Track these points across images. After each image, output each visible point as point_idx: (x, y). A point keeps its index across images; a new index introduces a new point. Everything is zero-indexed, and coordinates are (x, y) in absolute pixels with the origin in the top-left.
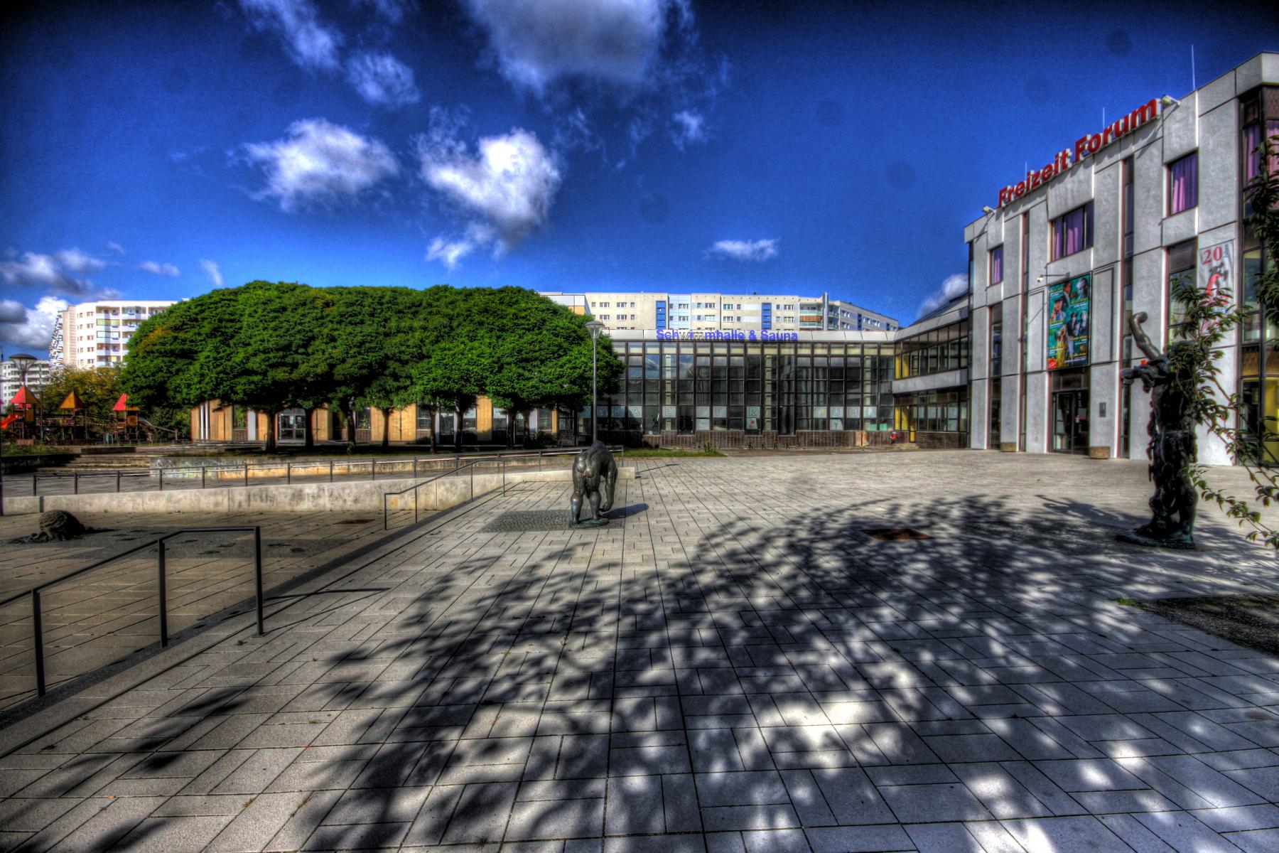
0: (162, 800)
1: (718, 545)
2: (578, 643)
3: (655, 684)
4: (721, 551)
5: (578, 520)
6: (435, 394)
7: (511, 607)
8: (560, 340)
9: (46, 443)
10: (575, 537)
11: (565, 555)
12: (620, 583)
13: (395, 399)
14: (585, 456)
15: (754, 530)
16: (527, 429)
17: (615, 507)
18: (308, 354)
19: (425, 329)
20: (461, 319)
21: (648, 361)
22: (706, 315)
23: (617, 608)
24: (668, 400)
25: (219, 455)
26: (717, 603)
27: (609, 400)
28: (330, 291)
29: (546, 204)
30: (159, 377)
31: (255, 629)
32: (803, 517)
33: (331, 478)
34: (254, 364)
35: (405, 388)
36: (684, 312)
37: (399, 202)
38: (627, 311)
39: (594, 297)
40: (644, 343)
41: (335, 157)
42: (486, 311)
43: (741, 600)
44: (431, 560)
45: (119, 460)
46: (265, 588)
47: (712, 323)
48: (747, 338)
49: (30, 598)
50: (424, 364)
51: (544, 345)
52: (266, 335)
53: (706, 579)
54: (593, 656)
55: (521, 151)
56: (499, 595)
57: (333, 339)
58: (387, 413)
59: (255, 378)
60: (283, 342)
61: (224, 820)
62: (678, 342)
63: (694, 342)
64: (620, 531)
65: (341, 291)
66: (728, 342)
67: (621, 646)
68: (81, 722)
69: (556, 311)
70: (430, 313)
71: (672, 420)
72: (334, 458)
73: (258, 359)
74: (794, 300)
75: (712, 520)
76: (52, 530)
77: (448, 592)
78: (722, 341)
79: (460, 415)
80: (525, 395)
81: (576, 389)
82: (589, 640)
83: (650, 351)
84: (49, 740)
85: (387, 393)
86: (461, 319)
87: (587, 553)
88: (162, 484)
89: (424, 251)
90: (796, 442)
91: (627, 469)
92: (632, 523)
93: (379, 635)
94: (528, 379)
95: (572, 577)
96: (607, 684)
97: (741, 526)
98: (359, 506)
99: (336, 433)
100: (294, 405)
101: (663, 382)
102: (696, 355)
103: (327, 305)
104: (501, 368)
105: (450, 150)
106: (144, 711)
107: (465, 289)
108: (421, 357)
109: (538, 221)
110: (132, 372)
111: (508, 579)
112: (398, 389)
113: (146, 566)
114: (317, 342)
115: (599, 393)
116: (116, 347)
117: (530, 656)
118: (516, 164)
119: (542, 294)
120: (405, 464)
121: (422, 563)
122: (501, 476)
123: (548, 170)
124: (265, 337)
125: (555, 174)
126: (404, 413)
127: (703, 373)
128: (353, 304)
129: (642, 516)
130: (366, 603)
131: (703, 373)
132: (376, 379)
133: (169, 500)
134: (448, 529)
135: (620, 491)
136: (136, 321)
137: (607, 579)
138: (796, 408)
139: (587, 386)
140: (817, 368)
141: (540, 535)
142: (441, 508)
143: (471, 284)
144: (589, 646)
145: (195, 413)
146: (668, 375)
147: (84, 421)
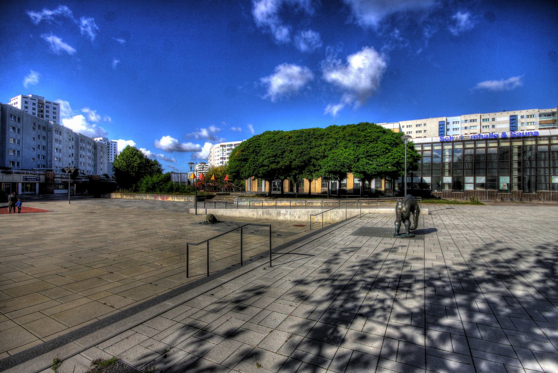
0: (244, 322)
1: (483, 256)
2: (403, 295)
3: (450, 327)
4: (487, 260)
5: (398, 234)
6: (330, 172)
7: (368, 272)
8: (387, 145)
9: (207, 191)
10: (398, 242)
11: (393, 250)
12: (424, 269)
13: (314, 175)
14: (402, 202)
15: (509, 249)
16: (370, 188)
17: (418, 228)
18: (283, 158)
19: (326, 144)
20: (341, 139)
21: (434, 153)
22: (465, 126)
23: (424, 281)
24: (447, 174)
25: (254, 197)
26: (487, 289)
27: (412, 174)
28: (291, 132)
29: (379, 80)
30: (237, 168)
31: (269, 264)
32: (548, 244)
33: (291, 207)
34: (266, 163)
35: (318, 170)
36: (456, 126)
37: (319, 91)
38: (421, 128)
39: (403, 123)
40: (432, 144)
41: (290, 77)
42: (352, 134)
43: (503, 289)
44: (330, 245)
45: (226, 198)
46: (272, 248)
47: (477, 130)
48: (500, 135)
49: (206, 243)
50: (325, 160)
51: (379, 148)
52: (269, 151)
53: (479, 274)
54: (413, 304)
55: (366, 57)
56: (362, 265)
57: (291, 151)
58: (310, 181)
59: (266, 168)
60: (275, 154)
61: (264, 336)
62: (453, 142)
63: (463, 141)
64: (422, 241)
65: (294, 132)
66: (486, 140)
67: (427, 302)
68: (220, 288)
69: (385, 132)
70: (328, 138)
71: (449, 184)
72: (291, 199)
73: (266, 161)
74: (536, 112)
75: (480, 241)
76: (210, 221)
77: (337, 261)
78: (482, 140)
79: (340, 182)
80: (369, 172)
81: (395, 169)
82: (409, 295)
83: (436, 148)
84: (212, 292)
85: (311, 172)
86: (341, 139)
87: (404, 250)
88: (238, 207)
89: (324, 111)
90: (537, 197)
91: (424, 210)
92: (427, 237)
93: (312, 275)
94: (371, 165)
95: (397, 262)
96: (424, 319)
97: (499, 246)
98: (301, 219)
99: (291, 189)
100: (278, 178)
101: (443, 164)
102: (464, 149)
103: (290, 138)
104: (358, 160)
105: (335, 65)
106: (237, 288)
107: (342, 126)
108: (325, 157)
109: (375, 89)
110: (230, 167)
111: (365, 258)
112: (315, 170)
113: (236, 236)
114: (286, 153)
115: (407, 171)
116: (225, 158)
117: (379, 297)
118: (363, 64)
119: (378, 124)
120: (317, 202)
121: (327, 246)
122: (359, 210)
123: (380, 62)
124: (268, 152)
125: (383, 64)
126: (316, 181)
127: (468, 159)
128: (299, 137)
129: (434, 234)
130: (307, 260)
131: (468, 159)
132: (306, 167)
133: (240, 212)
134: (337, 232)
135: (421, 221)
136: (231, 149)
137: (417, 265)
138: (536, 176)
139: (401, 167)
140: (553, 152)
141: (379, 239)
142: (332, 223)
143: (345, 123)
144: (409, 298)
145: (246, 181)
146: (447, 160)
147: (217, 184)
